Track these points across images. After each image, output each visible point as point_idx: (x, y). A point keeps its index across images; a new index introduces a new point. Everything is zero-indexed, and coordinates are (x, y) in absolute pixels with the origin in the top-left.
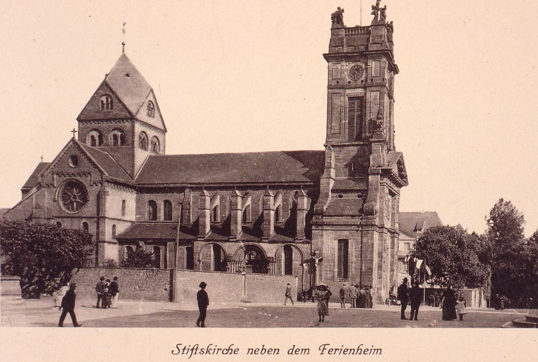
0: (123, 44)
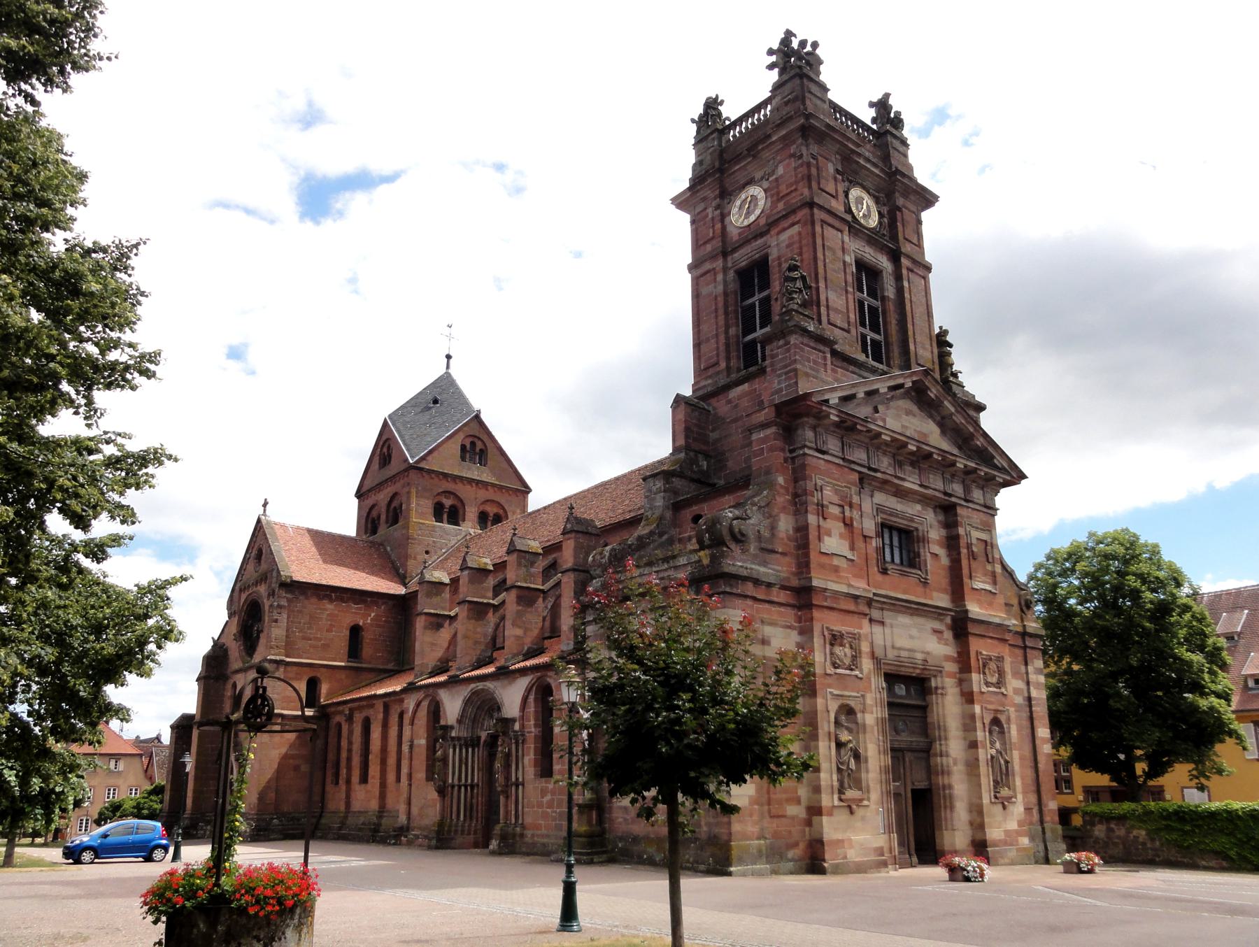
0: (449, 357)
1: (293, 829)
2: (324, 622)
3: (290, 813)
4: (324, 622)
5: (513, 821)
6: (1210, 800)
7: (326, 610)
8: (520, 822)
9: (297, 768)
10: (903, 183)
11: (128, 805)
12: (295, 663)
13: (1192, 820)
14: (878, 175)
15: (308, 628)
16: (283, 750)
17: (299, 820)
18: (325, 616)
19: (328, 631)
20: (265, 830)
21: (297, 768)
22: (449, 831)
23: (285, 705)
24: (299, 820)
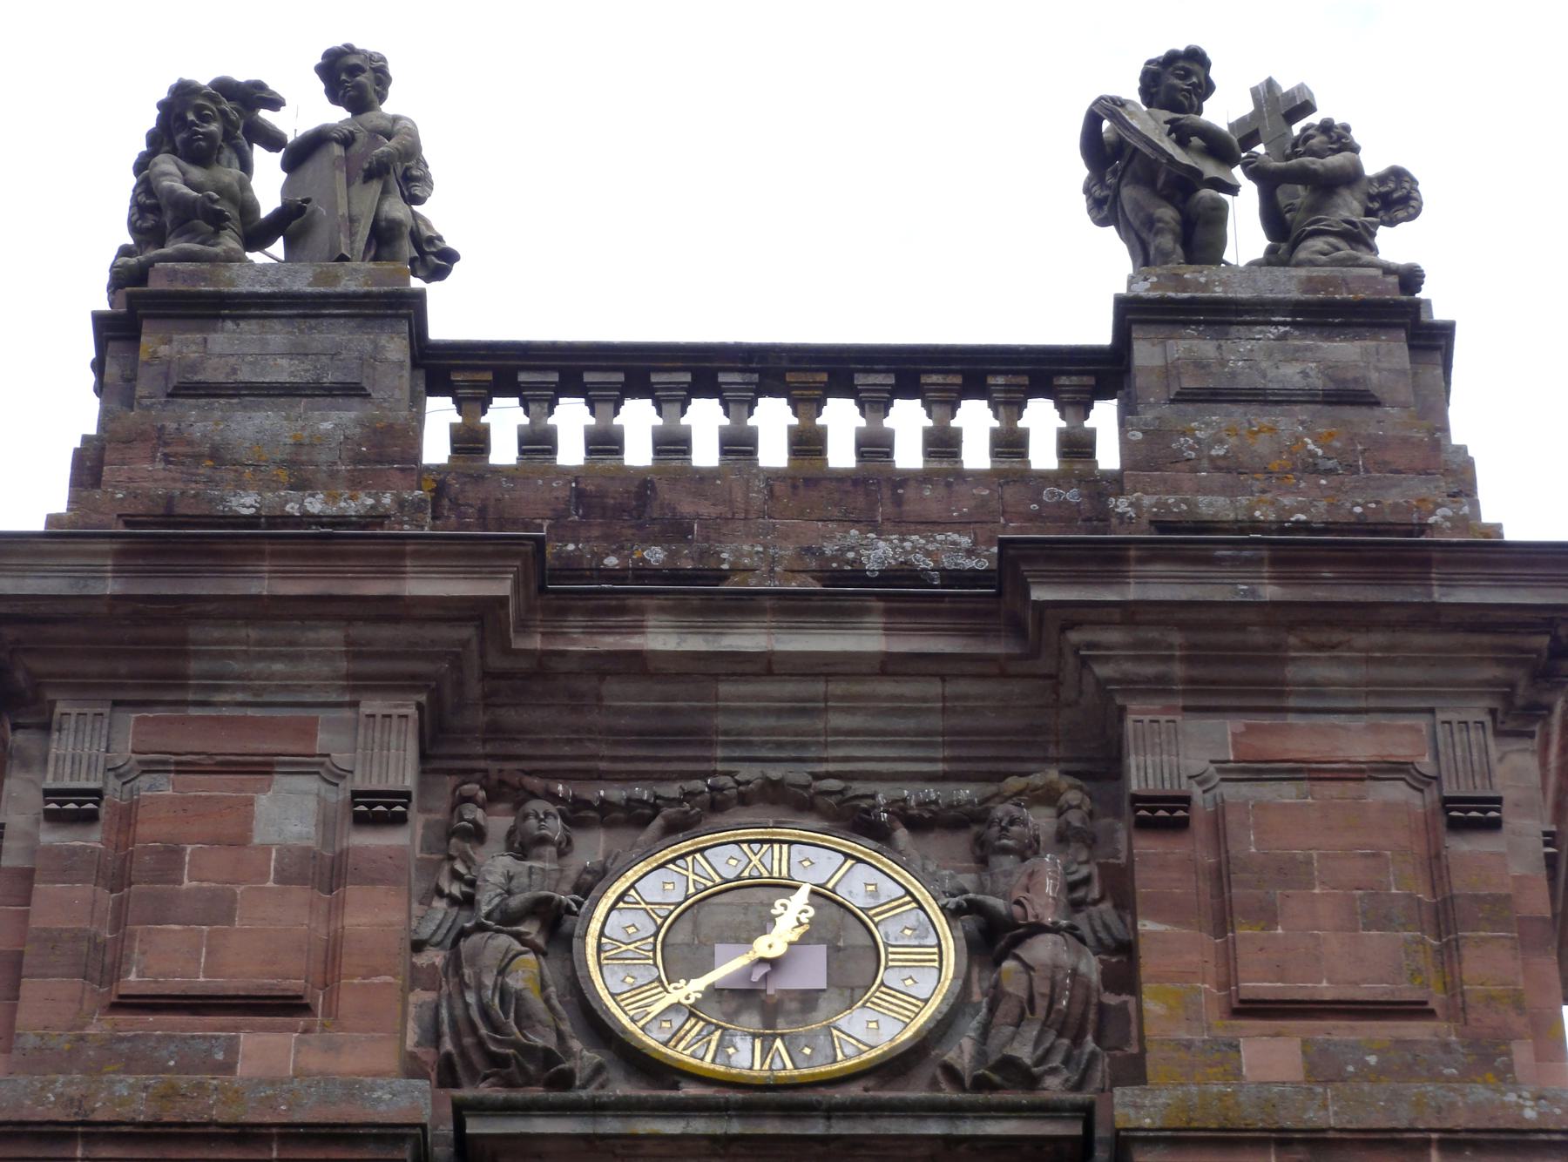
10: (1130, 613)
14: (889, 665)
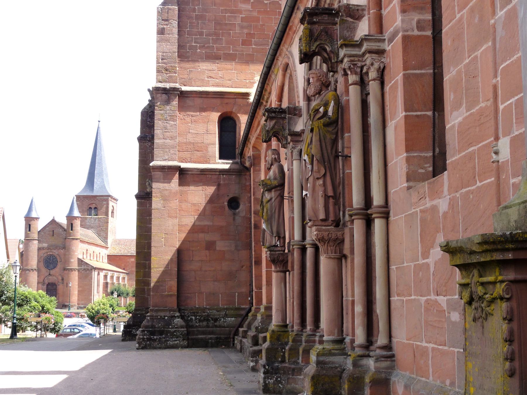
1: (204, 333)
2: (238, 30)
3: (204, 310)
4: (238, 30)
5: (360, 337)
6: (331, 253)
7: (240, 12)
8: (381, 340)
9: (210, 246)
11: (504, 300)
12: (196, 92)
13: (145, 154)
15: (215, 41)
16: (190, 221)
17: (216, 320)
18: (238, 21)
19: (244, 43)
20: (161, 333)
21: (210, 246)
22: (294, 351)
23: (187, 155)
24: (216, 320)
